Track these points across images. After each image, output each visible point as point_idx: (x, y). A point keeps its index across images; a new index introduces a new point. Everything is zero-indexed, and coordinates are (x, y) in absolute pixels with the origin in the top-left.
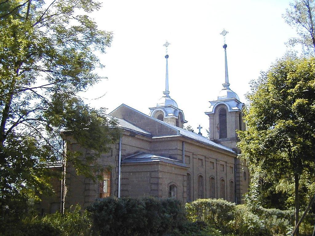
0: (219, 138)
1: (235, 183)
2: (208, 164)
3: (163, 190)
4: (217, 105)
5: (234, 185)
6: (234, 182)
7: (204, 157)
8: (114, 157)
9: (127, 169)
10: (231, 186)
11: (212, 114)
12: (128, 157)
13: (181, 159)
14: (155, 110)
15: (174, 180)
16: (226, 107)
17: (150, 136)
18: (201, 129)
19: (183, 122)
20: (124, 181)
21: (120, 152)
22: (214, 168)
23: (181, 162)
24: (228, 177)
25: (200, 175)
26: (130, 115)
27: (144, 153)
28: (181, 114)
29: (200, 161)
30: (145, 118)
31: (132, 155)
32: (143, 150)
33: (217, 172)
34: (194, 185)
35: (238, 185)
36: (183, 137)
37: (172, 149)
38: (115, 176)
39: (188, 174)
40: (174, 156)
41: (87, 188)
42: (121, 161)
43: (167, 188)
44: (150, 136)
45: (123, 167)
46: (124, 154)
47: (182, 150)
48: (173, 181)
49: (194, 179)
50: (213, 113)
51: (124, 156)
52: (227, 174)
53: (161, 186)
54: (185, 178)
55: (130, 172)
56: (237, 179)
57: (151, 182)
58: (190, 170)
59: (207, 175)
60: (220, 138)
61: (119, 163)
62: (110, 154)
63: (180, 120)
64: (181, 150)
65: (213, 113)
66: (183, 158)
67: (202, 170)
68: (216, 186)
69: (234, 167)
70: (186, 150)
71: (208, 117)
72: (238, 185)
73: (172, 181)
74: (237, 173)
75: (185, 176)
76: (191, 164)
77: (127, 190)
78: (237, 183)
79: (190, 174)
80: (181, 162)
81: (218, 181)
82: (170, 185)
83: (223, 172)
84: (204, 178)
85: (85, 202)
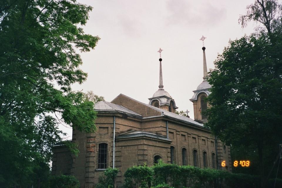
0: (201, 119)
1: (216, 154)
2: (201, 142)
3: (148, 160)
4: (197, 95)
5: (215, 156)
6: (215, 154)
7: (187, 133)
8: (109, 134)
9: (118, 144)
10: (213, 158)
11: (196, 100)
12: (122, 134)
13: (165, 135)
14: (152, 100)
15: (159, 152)
16: (205, 95)
17: (141, 117)
18: (188, 113)
19: (175, 108)
20: (118, 153)
21: (114, 130)
22: (196, 143)
23: (166, 137)
24: (209, 150)
25: (183, 148)
26: (126, 102)
27: (135, 131)
28: (172, 102)
29: (183, 137)
30: (137, 104)
31: (125, 132)
32: (135, 129)
33: (199, 145)
34: (178, 156)
35: (219, 156)
36: (166, 117)
37: (158, 127)
38: (111, 150)
39: (172, 148)
40: (160, 132)
41: (87, 161)
42: (115, 137)
43: (152, 159)
44: (141, 117)
45: (117, 142)
46: (118, 131)
47: (166, 128)
48: (158, 153)
49: (178, 151)
50: (196, 99)
51: (118, 133)
52: (209, 148)
53: (147, 157)
54: (169, 150)
55: (122, 146)
56: (218, 151)
57: (138, 154)
58: (173, 144)
59: (190, 148)
60: (202, 119)
61: (113, 139)
62: (106, 132)
63: (172, 106)
64: (165, 128)
65: (196, 99)
66: (167, 134)
67: (185, 145)
68: (199, 157)
69: (214, 142)
70: (170, 127)
71: (192, 103)
72: (219, 156)
73: (156, 152)
74: (217, 146)
75: (168, 149)
76: (175, 139)
77: (120, 161)
78: (218, 155)
79: (175, 147)
80: (166, 137)
81: (200, 153)
82: (155, 156)
83: (205, 146)
84: (187, 150)
85: (86, 172)
